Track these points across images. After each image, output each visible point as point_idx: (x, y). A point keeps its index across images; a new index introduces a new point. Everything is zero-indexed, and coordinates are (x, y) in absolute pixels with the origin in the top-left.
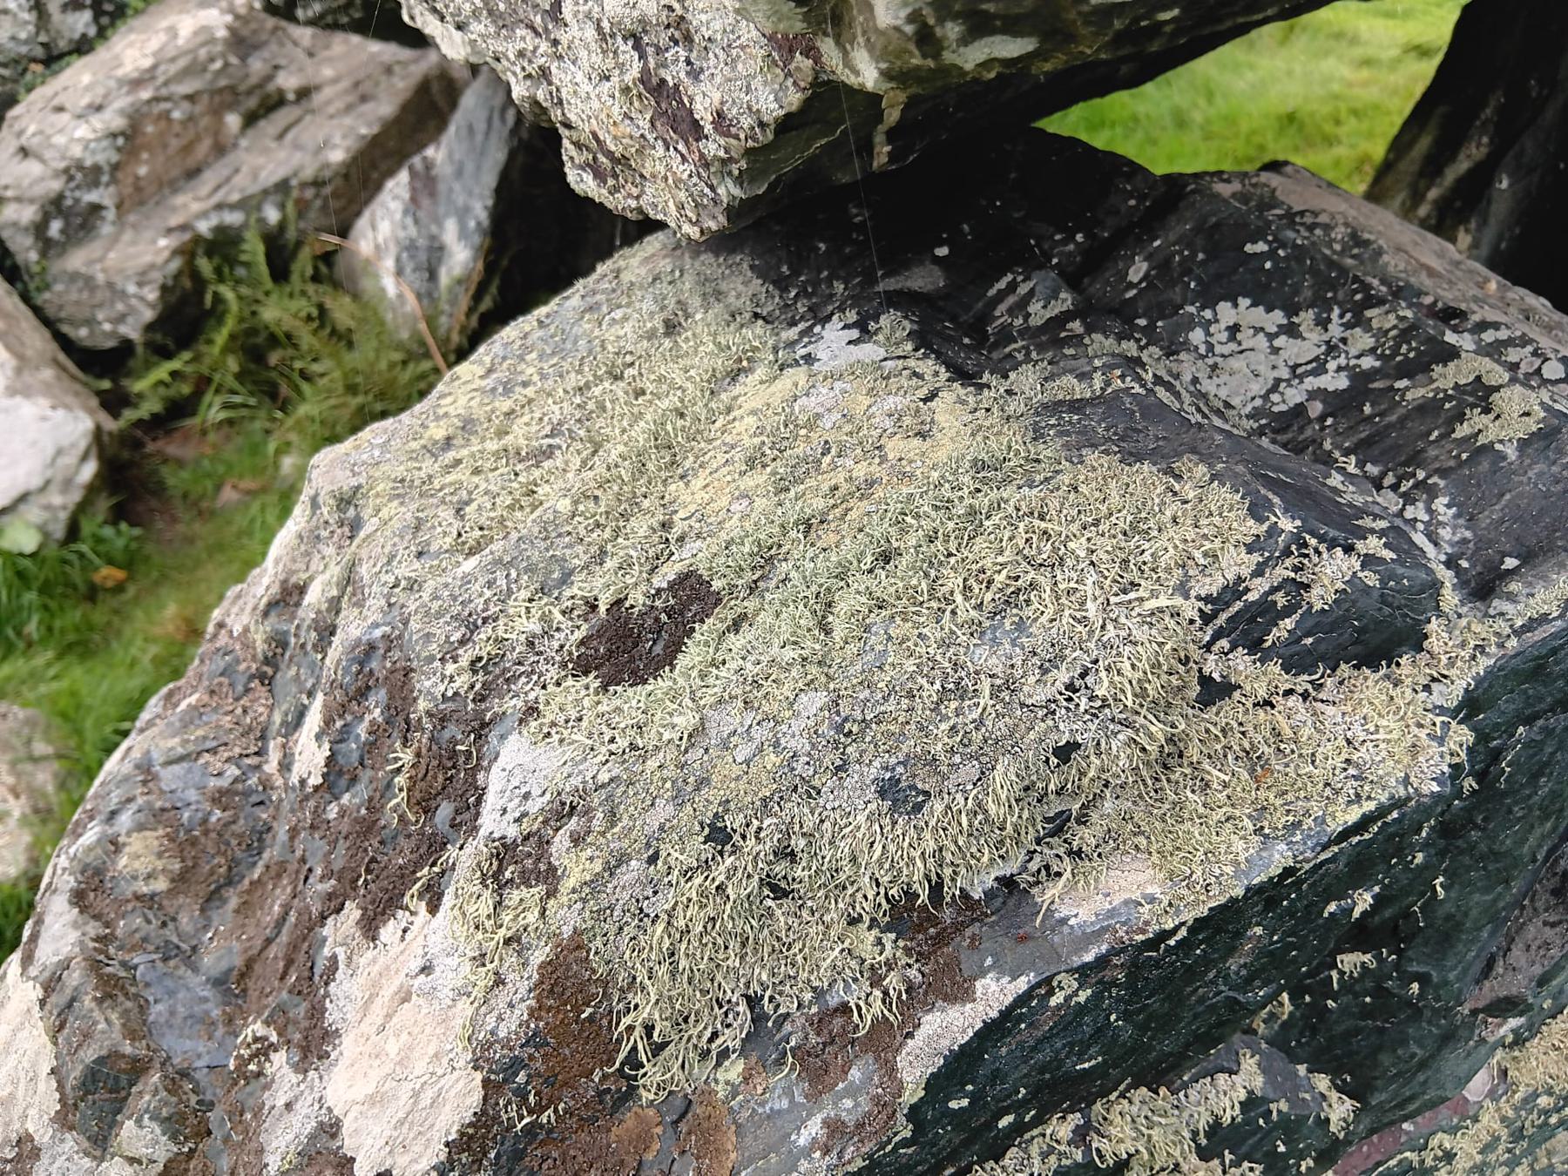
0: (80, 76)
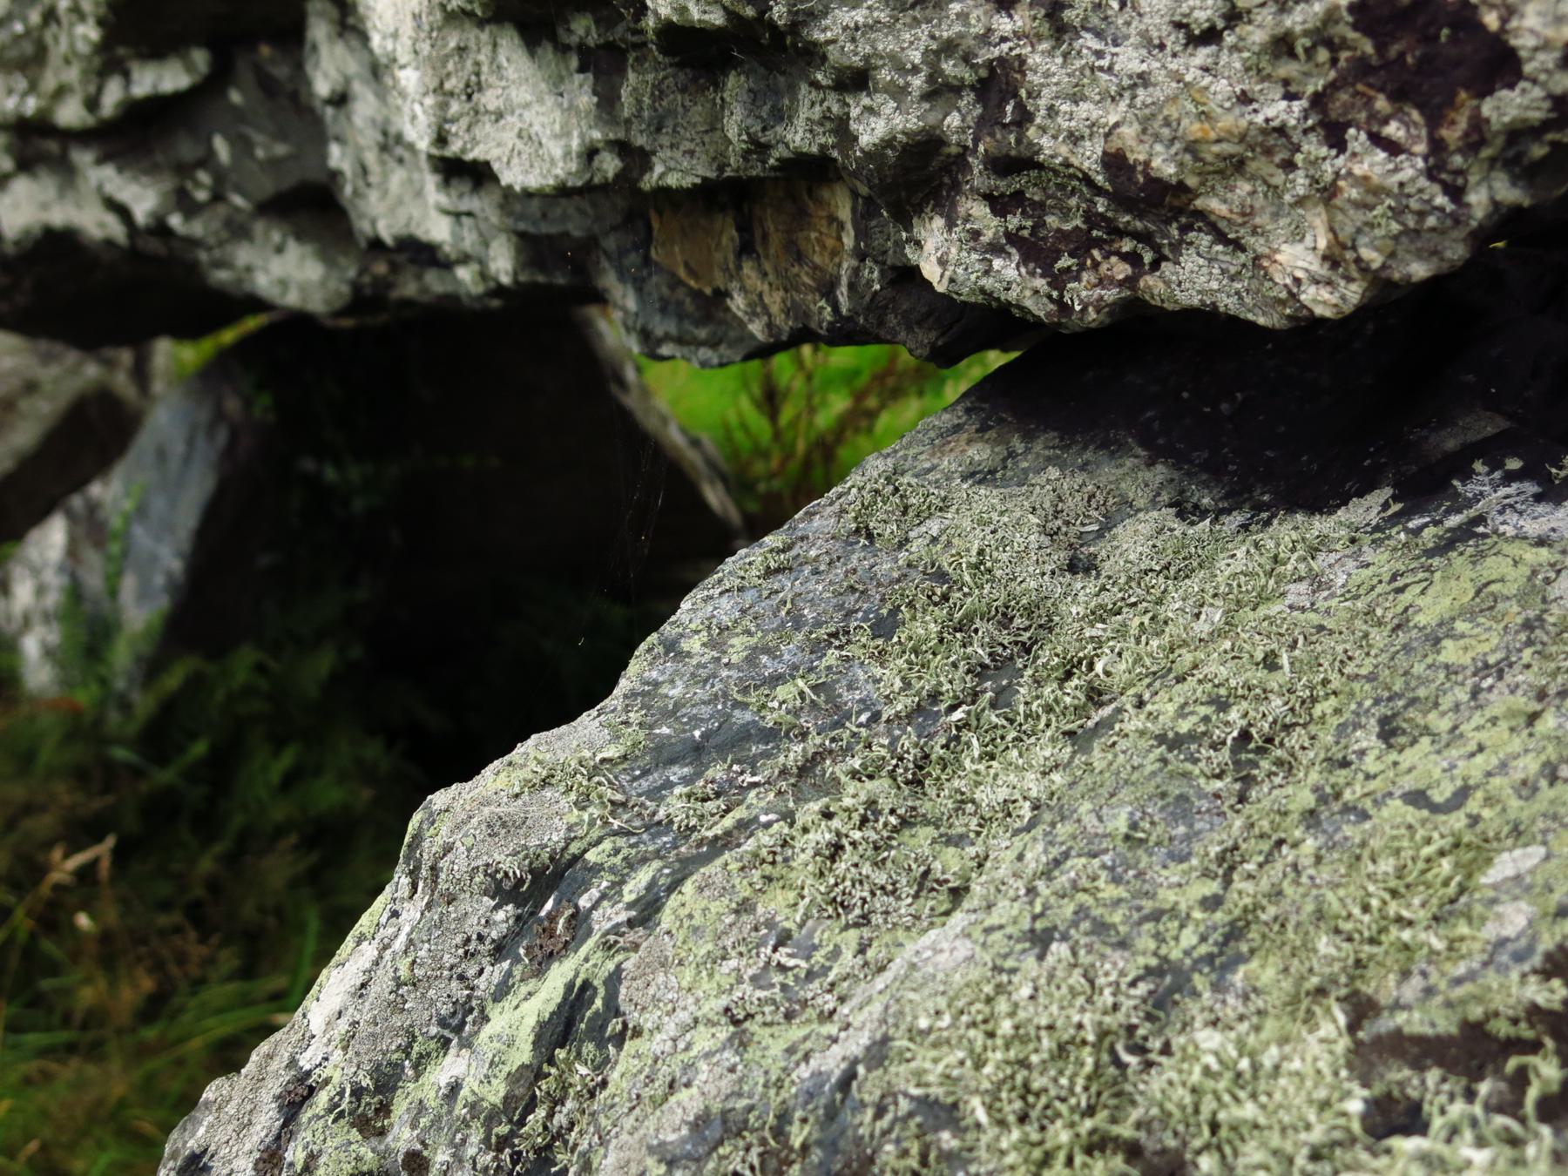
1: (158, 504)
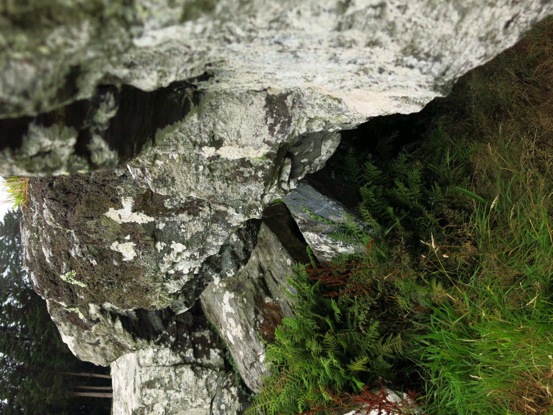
0: (240, 356)
1: (310, 204)
